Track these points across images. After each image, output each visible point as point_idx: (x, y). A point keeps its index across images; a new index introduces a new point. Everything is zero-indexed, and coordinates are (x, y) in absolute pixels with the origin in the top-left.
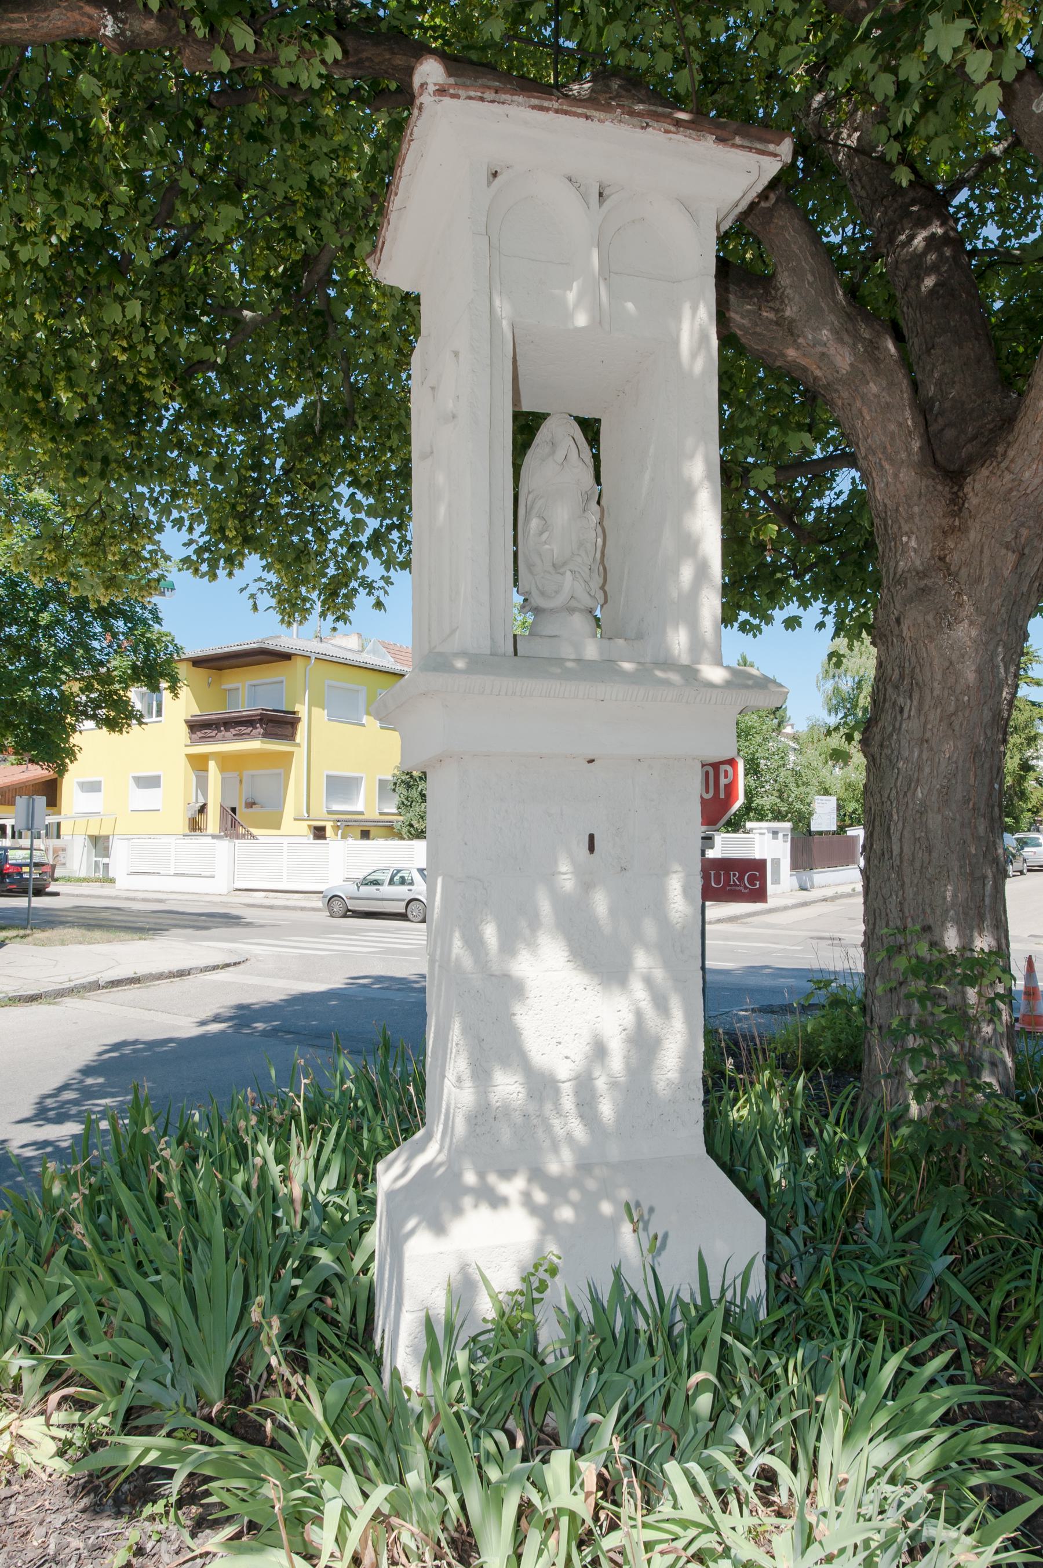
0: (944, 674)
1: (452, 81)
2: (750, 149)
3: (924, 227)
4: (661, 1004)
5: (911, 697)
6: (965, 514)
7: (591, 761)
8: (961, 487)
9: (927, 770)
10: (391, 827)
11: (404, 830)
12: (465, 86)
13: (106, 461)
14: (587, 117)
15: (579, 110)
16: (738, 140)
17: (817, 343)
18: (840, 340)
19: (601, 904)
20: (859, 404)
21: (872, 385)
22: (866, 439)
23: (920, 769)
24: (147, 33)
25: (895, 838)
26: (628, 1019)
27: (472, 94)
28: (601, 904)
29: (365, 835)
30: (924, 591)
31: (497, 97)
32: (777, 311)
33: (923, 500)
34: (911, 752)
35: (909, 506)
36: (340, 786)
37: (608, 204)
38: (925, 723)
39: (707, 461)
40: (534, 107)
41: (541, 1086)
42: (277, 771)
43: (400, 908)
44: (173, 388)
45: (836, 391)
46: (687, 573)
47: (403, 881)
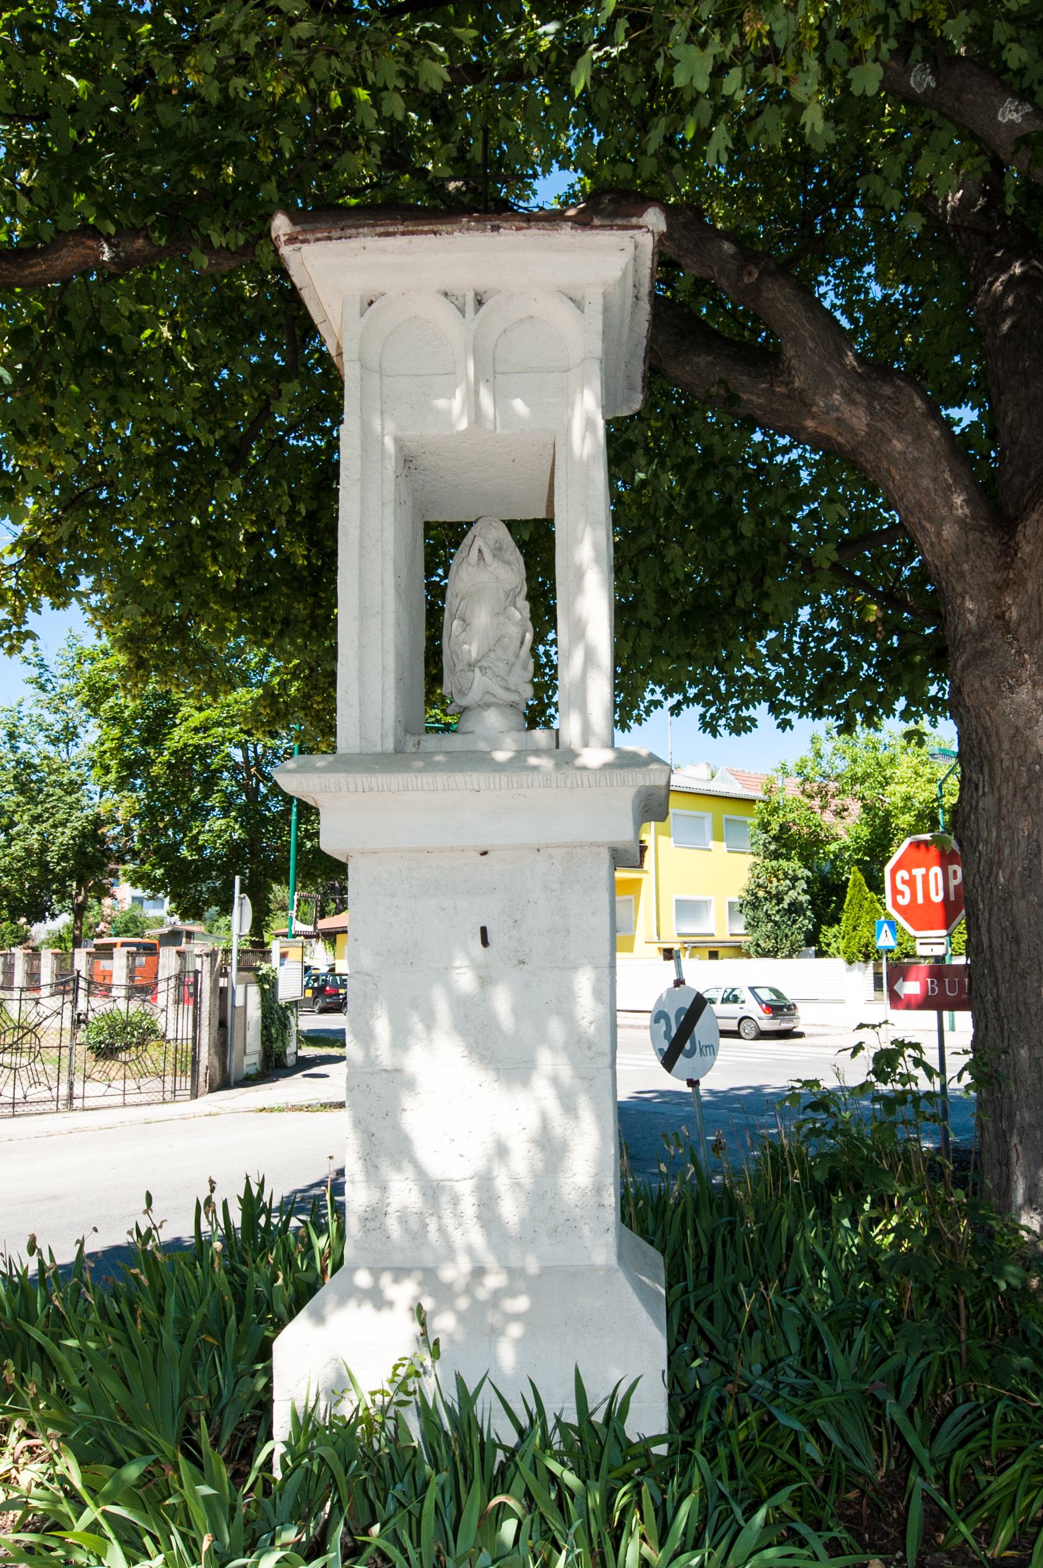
0: (1011, 742)
1: (298, 228)
2: (611, 227)
3: (1005, 271)
4: (570, 1109)
5: (981, 771)
6: (1019, 564)
7: (484, 853)
8: (1013, 536)
9: (1007, 851)
10: (740, 947)
11: (752, 950)
12: (313, 231)
13: (286, 622)
14: (435, 233)
15: (426, 228)
16: (596, 222)
17: (830, 408)
18: (852, 402)
19: (502, 1002)
20: (885, 464)
21: (895, 442)
22: (901, 499)
23: (1000, 850)
24: (138, 251)
25: (983, 930)
26: (533, 1122)
27: (319, 235)
28: (502, 1002)
29: (714, 955)
30: (982, 654)
31: (343, 234)
32: (787, 384)
33: (972, 555)
34: (989, 832)
35: (958, 564)
36: (687, 908)
37: (483, 309)
38: (1000, 799)
39: (595, 545)
40: (380, 235)
41: (433, 1191)
42: (628, 897)
43: (732, 1025)
44: (309, 551)
45: (862, 454)
46: (578, 659)
47: (736, 999)
